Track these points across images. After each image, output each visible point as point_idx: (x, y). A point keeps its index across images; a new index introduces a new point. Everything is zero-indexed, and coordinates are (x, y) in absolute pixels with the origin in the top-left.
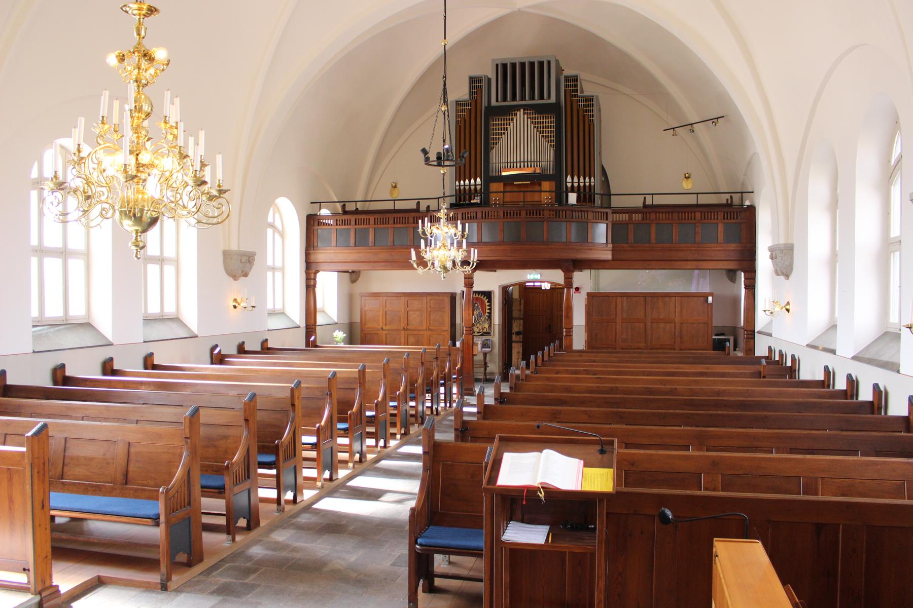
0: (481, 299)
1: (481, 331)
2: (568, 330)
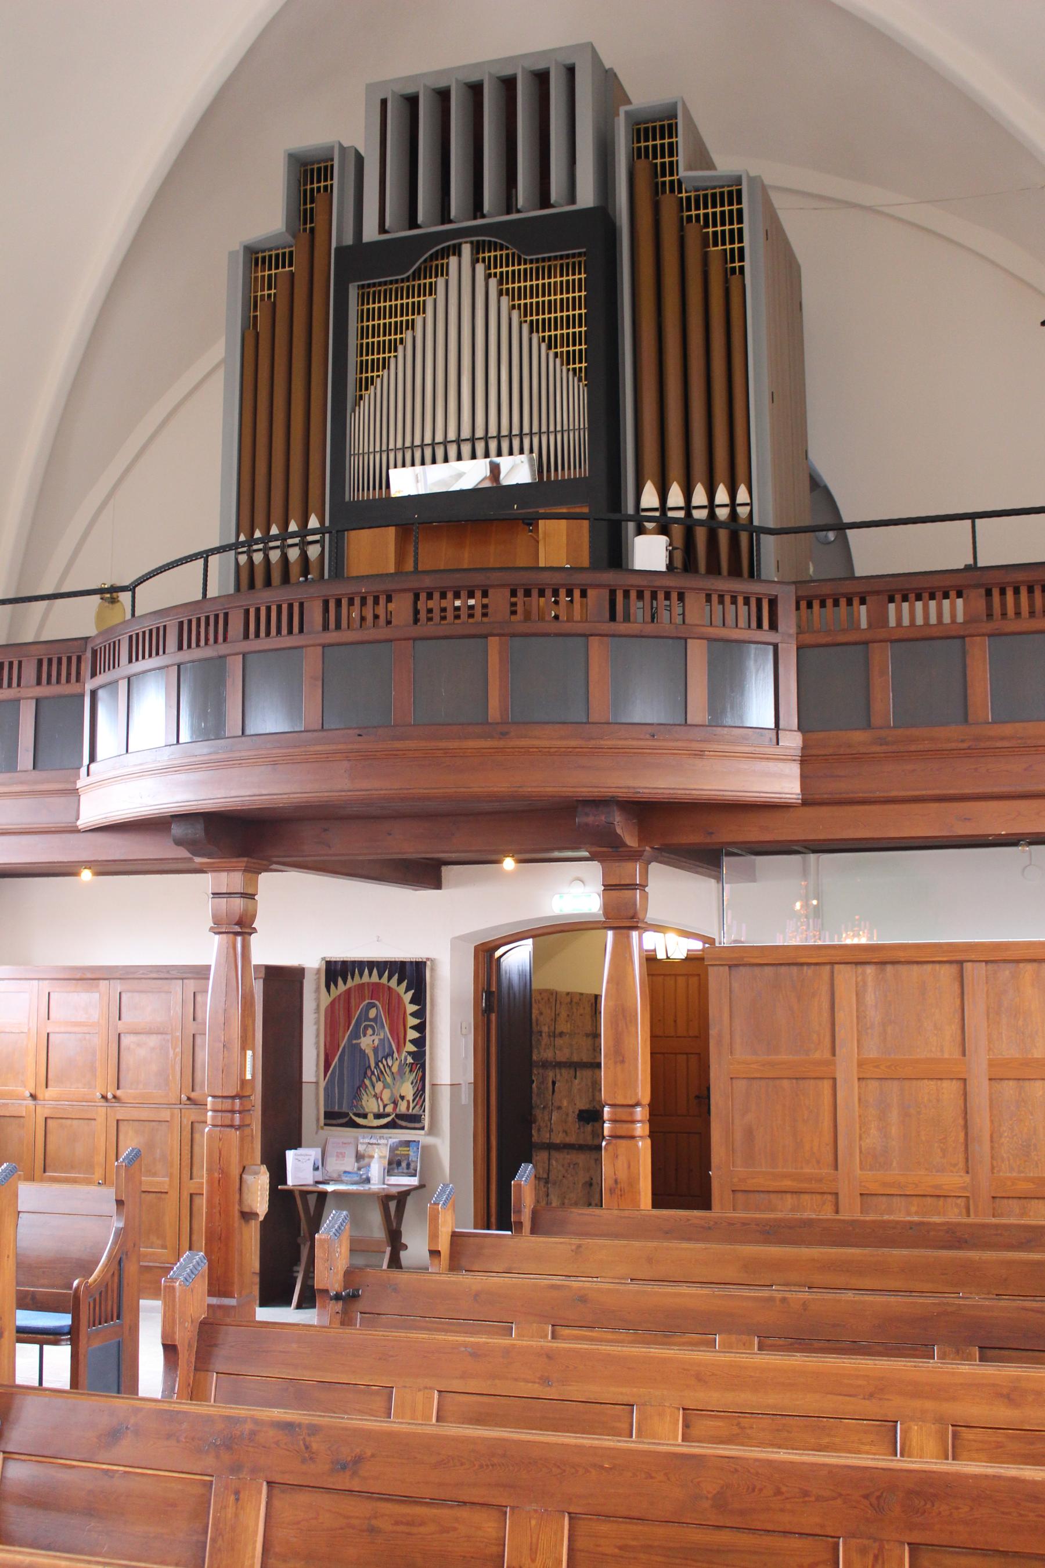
0: (389, 988)
1: (389, 1109)
2: (622, 1113)
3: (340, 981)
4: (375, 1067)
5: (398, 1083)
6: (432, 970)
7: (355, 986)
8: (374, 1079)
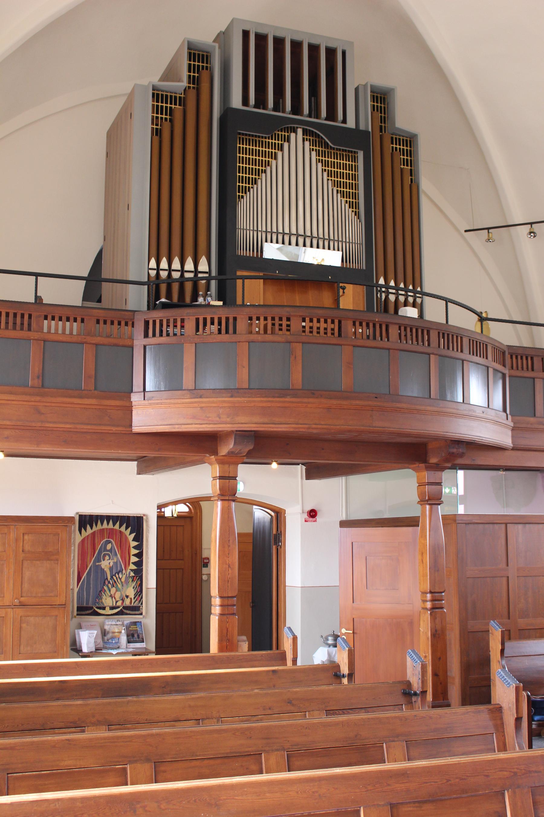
0: (120, 532)
1: (119, 604)
3: (88, 527)
4: (111, 579)
5: (125, 588)
6: (147, 522)
7: (98, 530)
8: (110, 586)
